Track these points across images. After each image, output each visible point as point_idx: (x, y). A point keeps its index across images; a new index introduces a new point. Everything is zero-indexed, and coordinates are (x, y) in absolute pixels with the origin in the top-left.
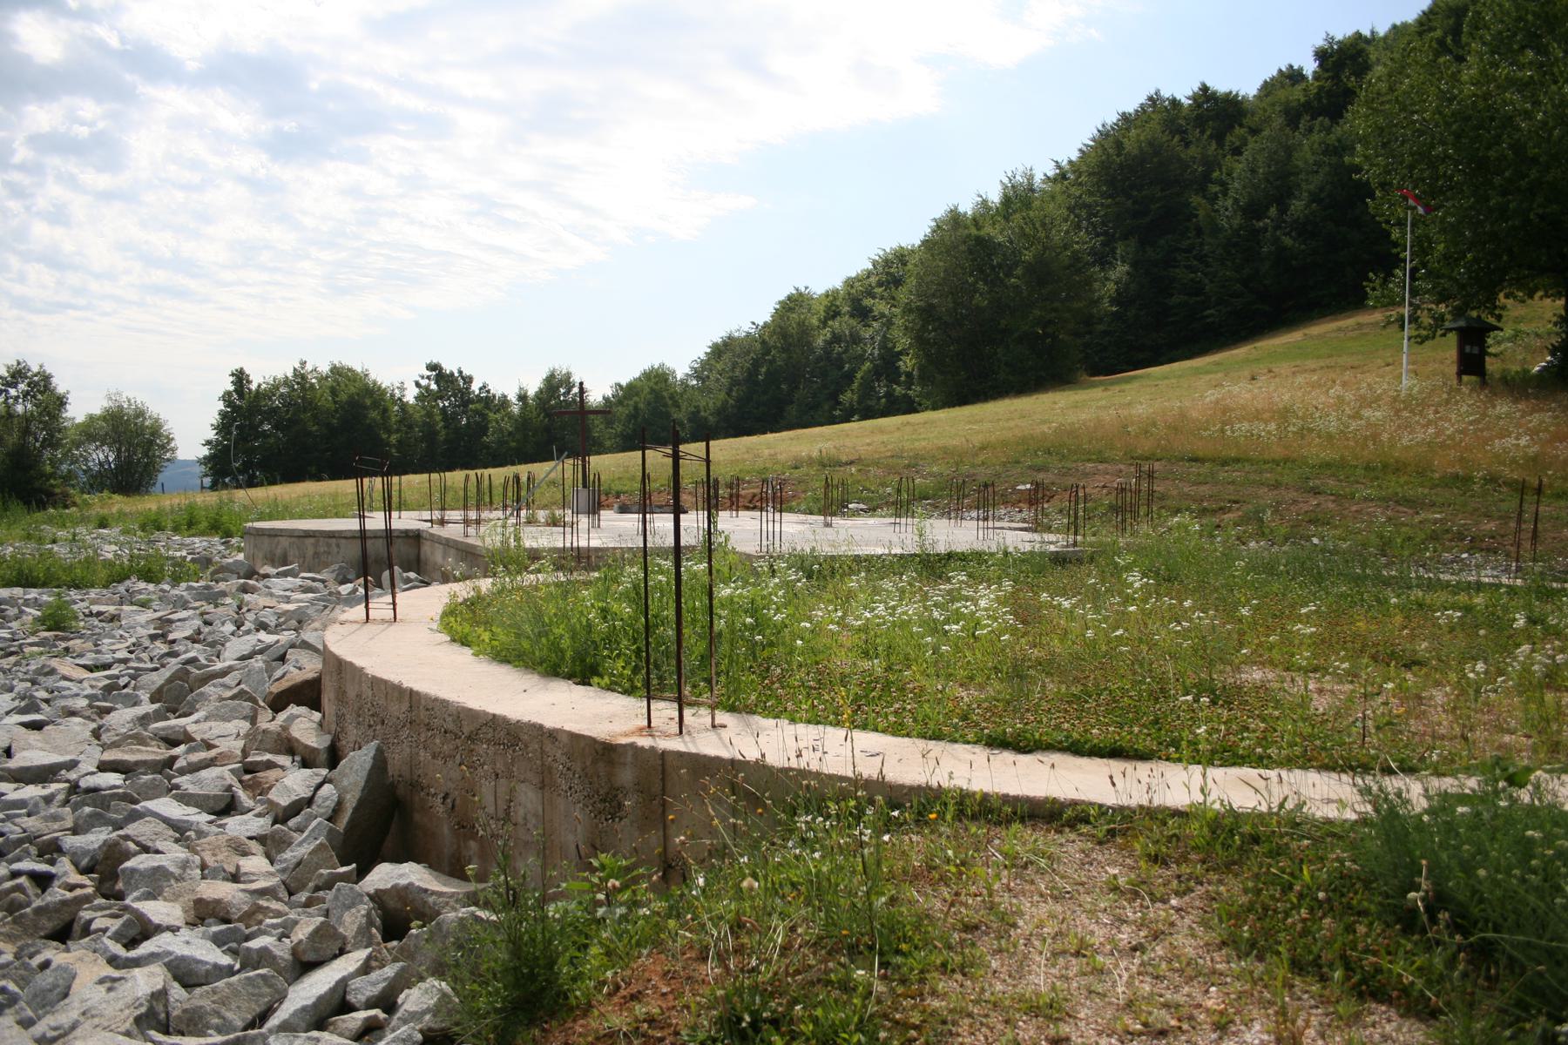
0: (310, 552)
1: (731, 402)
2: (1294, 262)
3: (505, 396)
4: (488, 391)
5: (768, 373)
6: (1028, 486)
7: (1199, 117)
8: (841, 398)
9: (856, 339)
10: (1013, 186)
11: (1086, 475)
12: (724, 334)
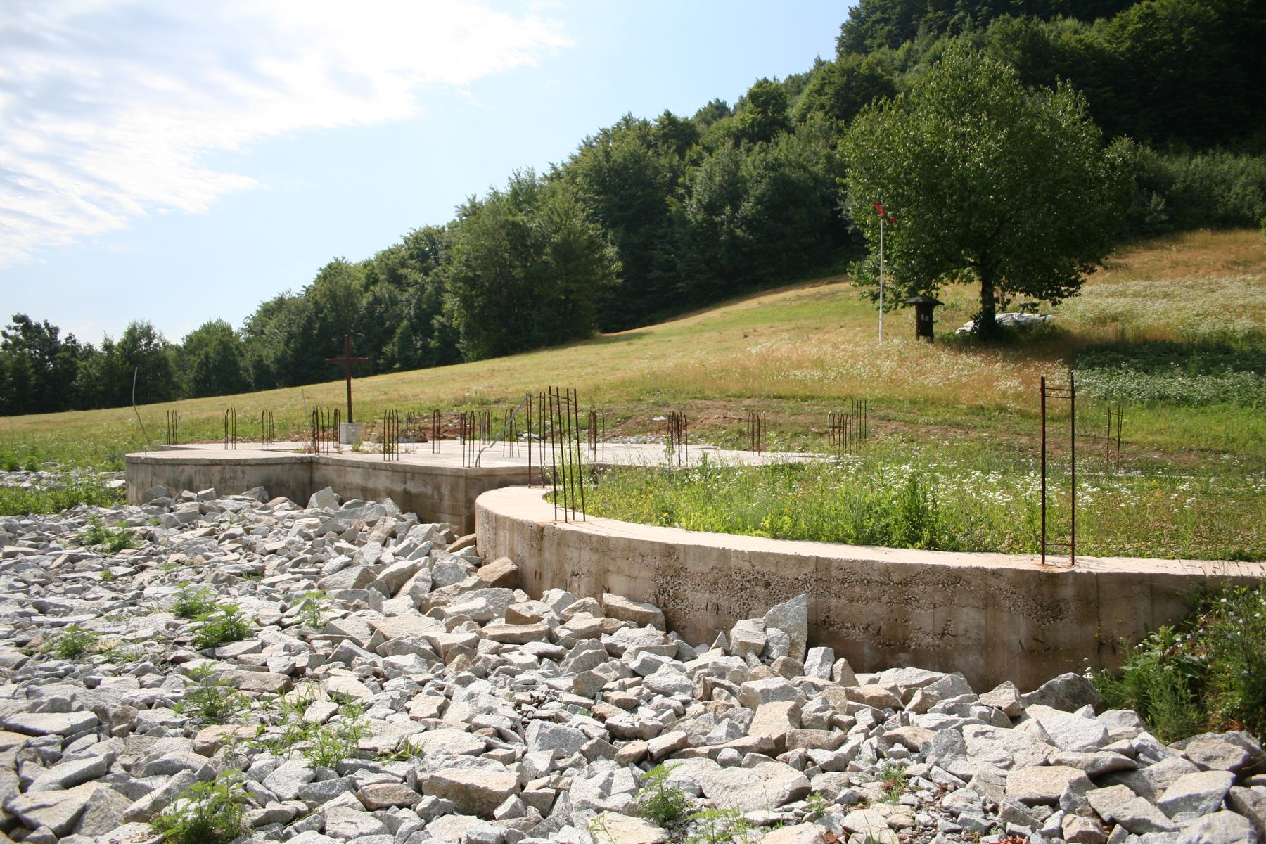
0: (217, 478)
1: (290, 352)
2: (744, 249)
3: (90, 346)
4: (74, 342)
5: (321, 329)
6: (662, 418)
7: (664, 135)
8: (384, 349)
9: (394, 301)
10: (519, 182)
11: (701, 410)
12: (277, 296)
